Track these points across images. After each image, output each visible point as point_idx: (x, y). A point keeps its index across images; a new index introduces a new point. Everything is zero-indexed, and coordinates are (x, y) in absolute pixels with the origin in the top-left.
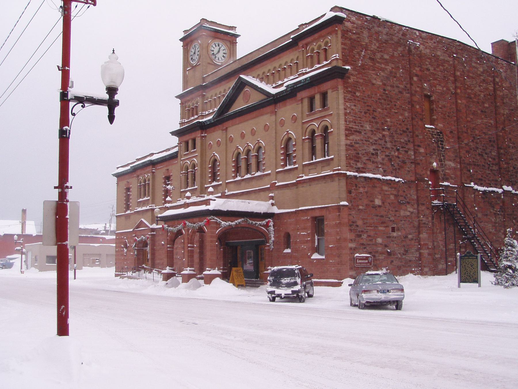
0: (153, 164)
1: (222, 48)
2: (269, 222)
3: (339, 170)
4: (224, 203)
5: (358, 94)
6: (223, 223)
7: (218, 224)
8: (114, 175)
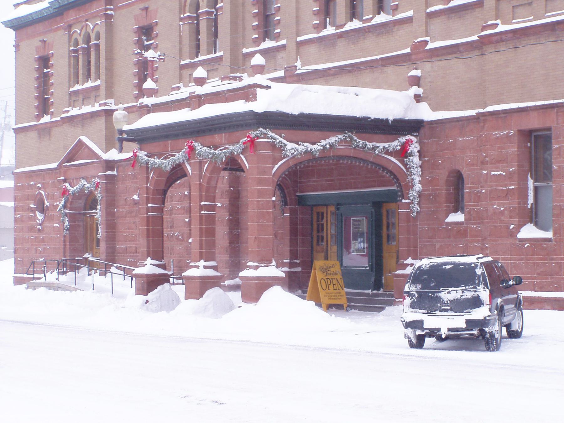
2: (408, 142)
6: (290, 146)
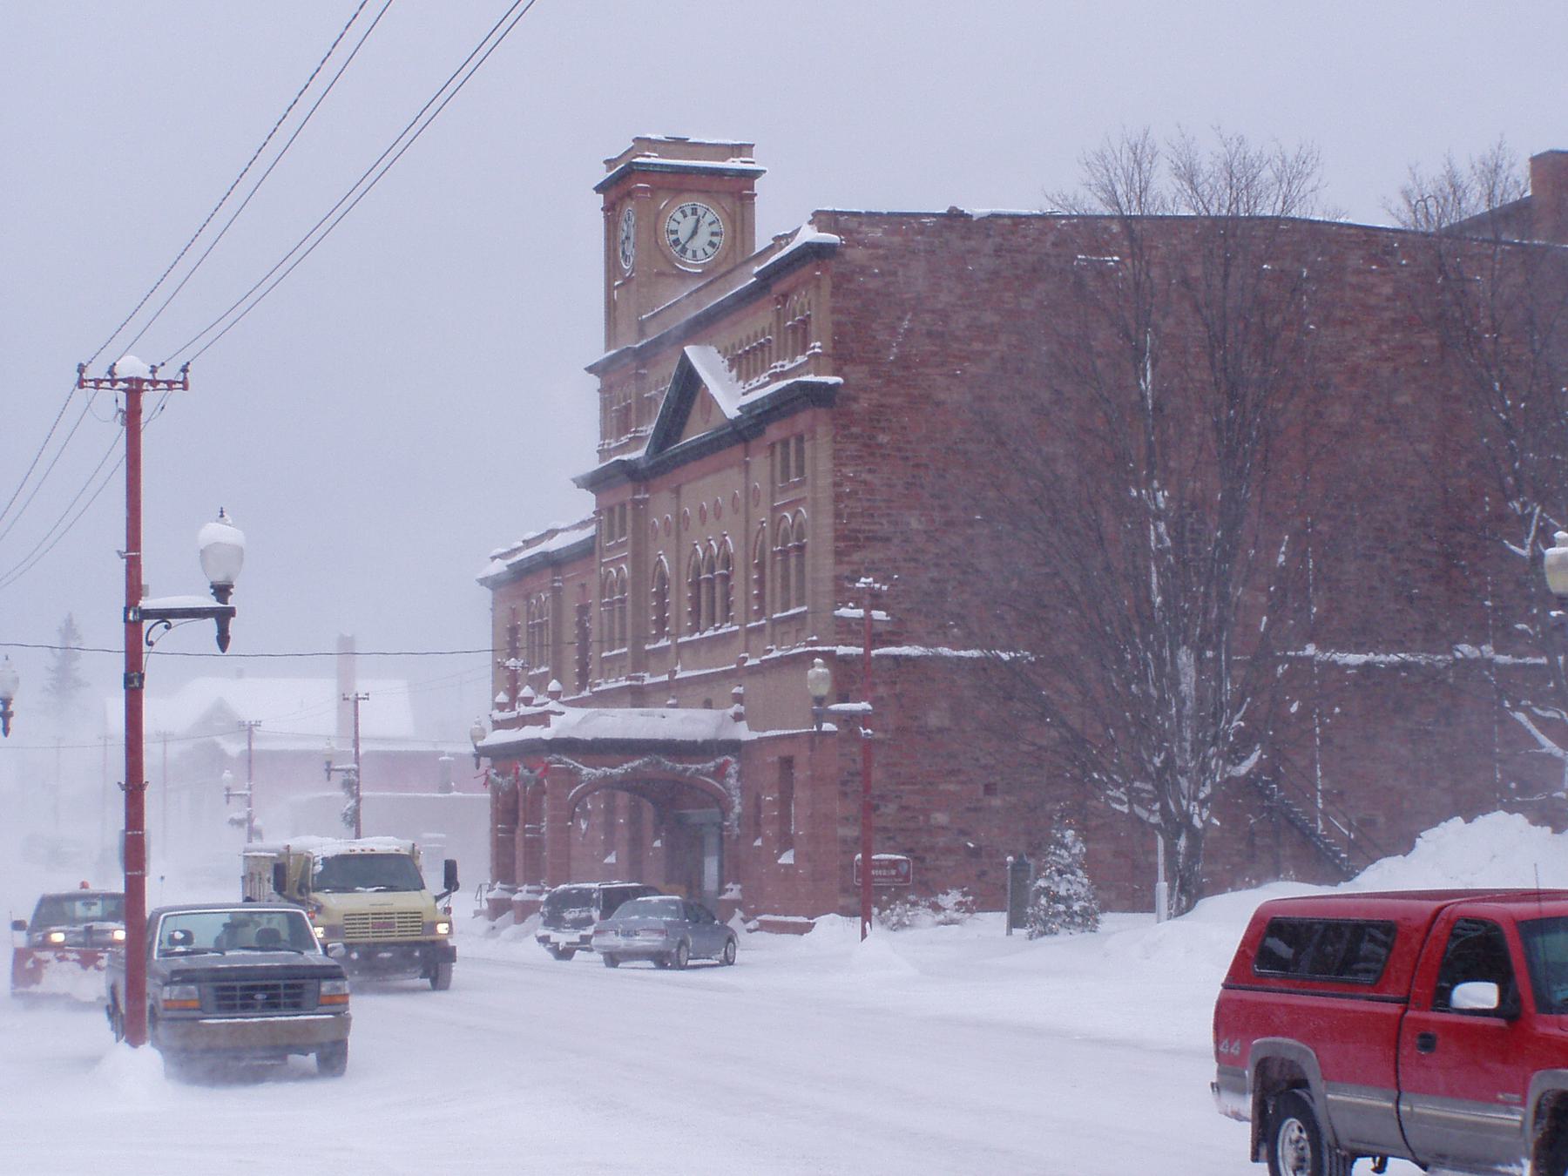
0: (553, 562)
1: (709, 218)
2: (726, 763)
3: (813, 644)
4: (585, 720)
5: (883, 438)
6: (586, 771)
7: (573, 774)
8: (483, 582)
